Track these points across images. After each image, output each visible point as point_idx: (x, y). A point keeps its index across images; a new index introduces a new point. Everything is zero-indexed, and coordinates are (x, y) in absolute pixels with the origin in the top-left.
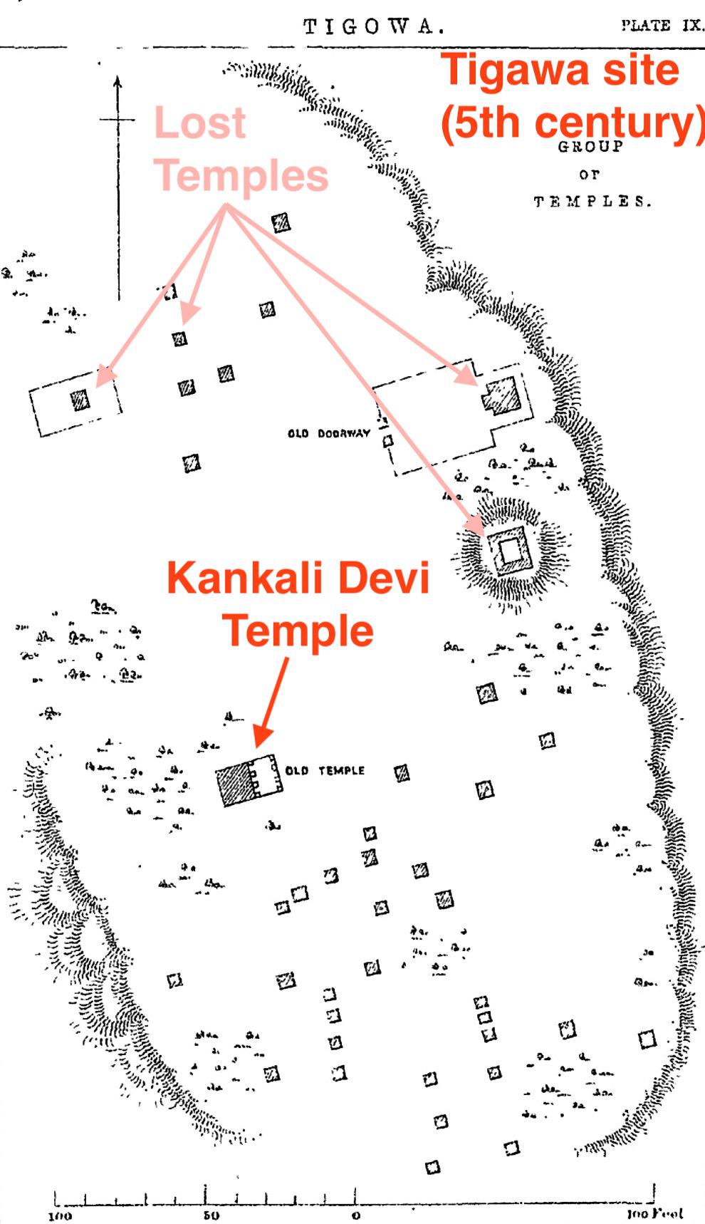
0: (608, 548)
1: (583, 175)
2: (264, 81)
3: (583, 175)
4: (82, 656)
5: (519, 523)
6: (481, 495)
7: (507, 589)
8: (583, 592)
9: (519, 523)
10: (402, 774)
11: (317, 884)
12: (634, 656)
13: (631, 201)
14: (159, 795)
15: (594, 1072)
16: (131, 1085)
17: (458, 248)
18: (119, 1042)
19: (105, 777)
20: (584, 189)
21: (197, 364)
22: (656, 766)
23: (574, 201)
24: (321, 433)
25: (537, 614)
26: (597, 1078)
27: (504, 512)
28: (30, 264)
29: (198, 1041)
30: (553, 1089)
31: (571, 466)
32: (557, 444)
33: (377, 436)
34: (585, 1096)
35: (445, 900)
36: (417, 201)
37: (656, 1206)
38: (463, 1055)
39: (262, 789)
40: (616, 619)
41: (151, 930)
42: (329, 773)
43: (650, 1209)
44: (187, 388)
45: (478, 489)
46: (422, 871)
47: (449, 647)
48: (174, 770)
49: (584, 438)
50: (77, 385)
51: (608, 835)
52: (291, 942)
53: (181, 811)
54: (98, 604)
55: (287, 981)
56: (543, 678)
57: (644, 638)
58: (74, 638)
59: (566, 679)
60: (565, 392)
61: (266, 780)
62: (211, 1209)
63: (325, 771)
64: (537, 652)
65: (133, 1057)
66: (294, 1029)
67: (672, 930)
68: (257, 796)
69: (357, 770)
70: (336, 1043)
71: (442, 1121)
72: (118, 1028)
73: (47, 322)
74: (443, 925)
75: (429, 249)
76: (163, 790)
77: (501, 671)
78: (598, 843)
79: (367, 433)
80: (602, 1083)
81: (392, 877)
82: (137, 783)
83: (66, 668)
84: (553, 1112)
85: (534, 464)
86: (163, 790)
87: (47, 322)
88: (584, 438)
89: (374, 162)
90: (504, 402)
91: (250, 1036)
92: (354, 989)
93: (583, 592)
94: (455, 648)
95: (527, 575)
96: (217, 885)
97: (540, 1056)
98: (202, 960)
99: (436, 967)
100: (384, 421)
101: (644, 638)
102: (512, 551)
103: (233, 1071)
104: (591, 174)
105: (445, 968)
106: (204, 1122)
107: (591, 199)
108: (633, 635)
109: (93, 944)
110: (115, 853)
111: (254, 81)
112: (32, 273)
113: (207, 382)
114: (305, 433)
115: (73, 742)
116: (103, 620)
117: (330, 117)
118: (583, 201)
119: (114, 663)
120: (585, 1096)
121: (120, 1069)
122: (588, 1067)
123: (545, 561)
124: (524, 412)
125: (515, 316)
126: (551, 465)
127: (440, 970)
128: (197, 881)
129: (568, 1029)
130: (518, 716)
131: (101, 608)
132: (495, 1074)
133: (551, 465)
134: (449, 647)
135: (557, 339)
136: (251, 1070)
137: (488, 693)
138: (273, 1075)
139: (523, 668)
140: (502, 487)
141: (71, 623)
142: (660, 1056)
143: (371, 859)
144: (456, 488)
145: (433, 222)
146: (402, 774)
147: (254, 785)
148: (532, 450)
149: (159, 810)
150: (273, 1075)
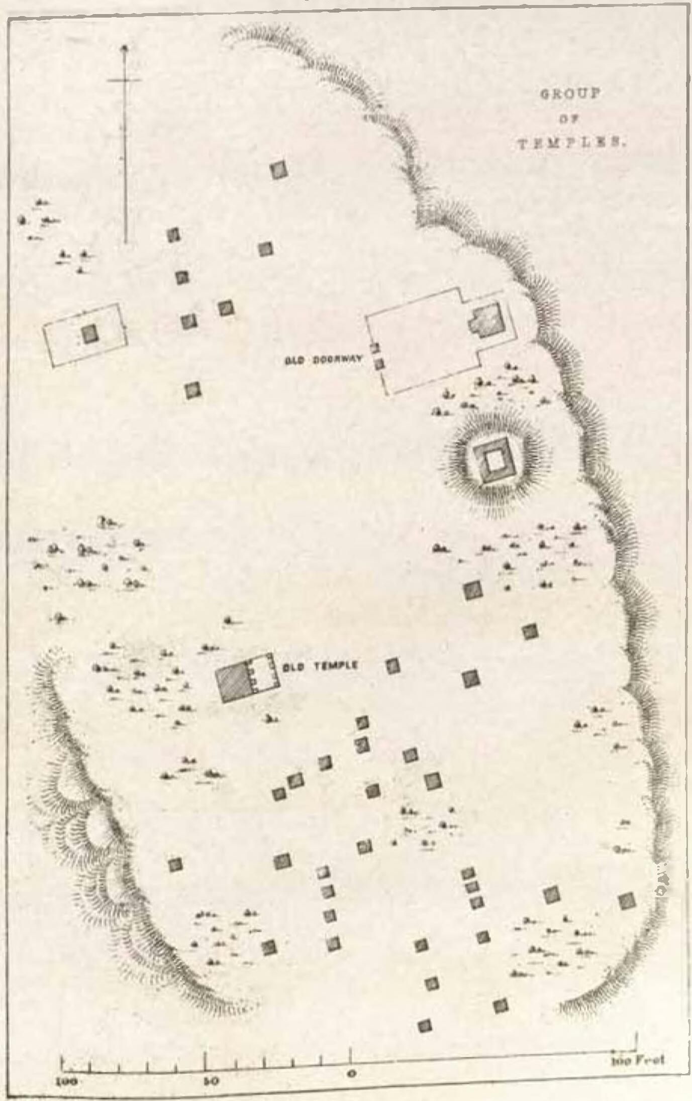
0: (586, 455)
1: (563, 119)
2: (263, 43)
3: (563, 119)
4: (90, 568)
5: (502, 435)
6: (468, 410)
7: (489, 493)
8: (561, 494)
9: (502, 435)
10: (393, 666)
11: (311, 772)
12: (610, 549)
13: (608, 141)
14: (161, 694)
15: (577, 933)
16: (133, 963)
17: (445, 190)
18: (122, 921)
19: (107, 678)
20: (563, 131)
21: (200, 297)
22: (631, 651)
23: (553, 144)
24: (316, 360)
25: (523, 513)
26: (579, 939)
27: (489, 425)
28: (44, 212)
29: (198, 920)
30: (540, 950)
31: (551, 380)
32: (540, 362)
33: (369, 360)
34: (568, 954)
35: (434, 781)
36: (409, 155)
37: (639, 1052)
38: (451, 922)
39: (259, 686)
40: (593, 518)
41: (156, 822)
42: (324, 667)
43: (633, 1057)
44: (189, 322)
45: (465, 405)
46: (411, 756)
47: (438, 549)
48: (176, 672)
49: (563, 360)
50: (86, 321)
51: (587, 717)
52: (288, 826)
53: (182, 709)
54: (103, 519)
55: (283, 861)
56: (527, 571)
57: (620, 539)
58: (84, 551)
59: (547, 575)
60: (543, 317)
61: (262, 675)
62: (209, 1076)
63: (320, 666)
64: (520, 551)
65: (135, 935)
66: (293, 911)
67: (648, 802)
68: (258, 691)
69: (350, 665)
70: (331, 916)
71: (433, 984)
72: (121, 909)
73: (59, 263)
74: (432, 805)
75: (416, 190)
76: (165, 689)
77: (488, 572)
78: (578, 725)
79: (359, 358)
80: (585, 943)
81: (382, 766)
82: (139, 684)
83: (74, 578)
84: (538, 970)
85: (516, 380)
86: (165, 689)
87: (59, 263)
88: (563, 360)
89: (368, 112)
90: (487, 325)
91: (248, 914)
92: (350, 869)
93: (561, 494)
94: (444, 550)
95: (510, 481)
96: (216, 775)
97: (527, 921)
98: (202, 849)
99: (425, 843)
100: (376, 348)
101: (620, 539)
102: (496, 461)
103: (235, 946)
104: (570, 119)
105: (434, 843)
106: (201, 993)
107: (571, 140)
108: (610, 532)
109: (97, 829)
110: (124, 754)
111: (254, 42)
112: (47, 220)
113: (208, 314)
114: (301, 360)
115: (80, 644)
116: (107, 535)
117: (326, 74)
118: (563, 143)
119: (119, 572)
120: (568, 954)
121: (122, 949)
122: (571, 928)
123: (527, 473)
124: (508, 334)
125: (499, 248)
126: (534, 381)
127: (430, 846)
128: (198, 773)
129: (552, 895)
130: (502, 611)
131: (106, 522)
132: (484, 937)
133: (534, 381)
134: (438, 549)
135: (538, 265)
136: (252, 946)
137: (472, 590)
138: (270, 947)
139: (507, 567)
140: (487, 403)
141: (79, 537)
142: (638, 916)
143: (363, 746)
144: (445, 405)
145: (422, 166)
146: (393, 666)
147: (252, 682)
148: (516, 368)
149: (163, 708)
150: (270, 947)
